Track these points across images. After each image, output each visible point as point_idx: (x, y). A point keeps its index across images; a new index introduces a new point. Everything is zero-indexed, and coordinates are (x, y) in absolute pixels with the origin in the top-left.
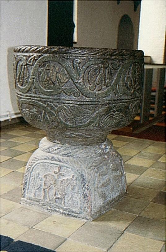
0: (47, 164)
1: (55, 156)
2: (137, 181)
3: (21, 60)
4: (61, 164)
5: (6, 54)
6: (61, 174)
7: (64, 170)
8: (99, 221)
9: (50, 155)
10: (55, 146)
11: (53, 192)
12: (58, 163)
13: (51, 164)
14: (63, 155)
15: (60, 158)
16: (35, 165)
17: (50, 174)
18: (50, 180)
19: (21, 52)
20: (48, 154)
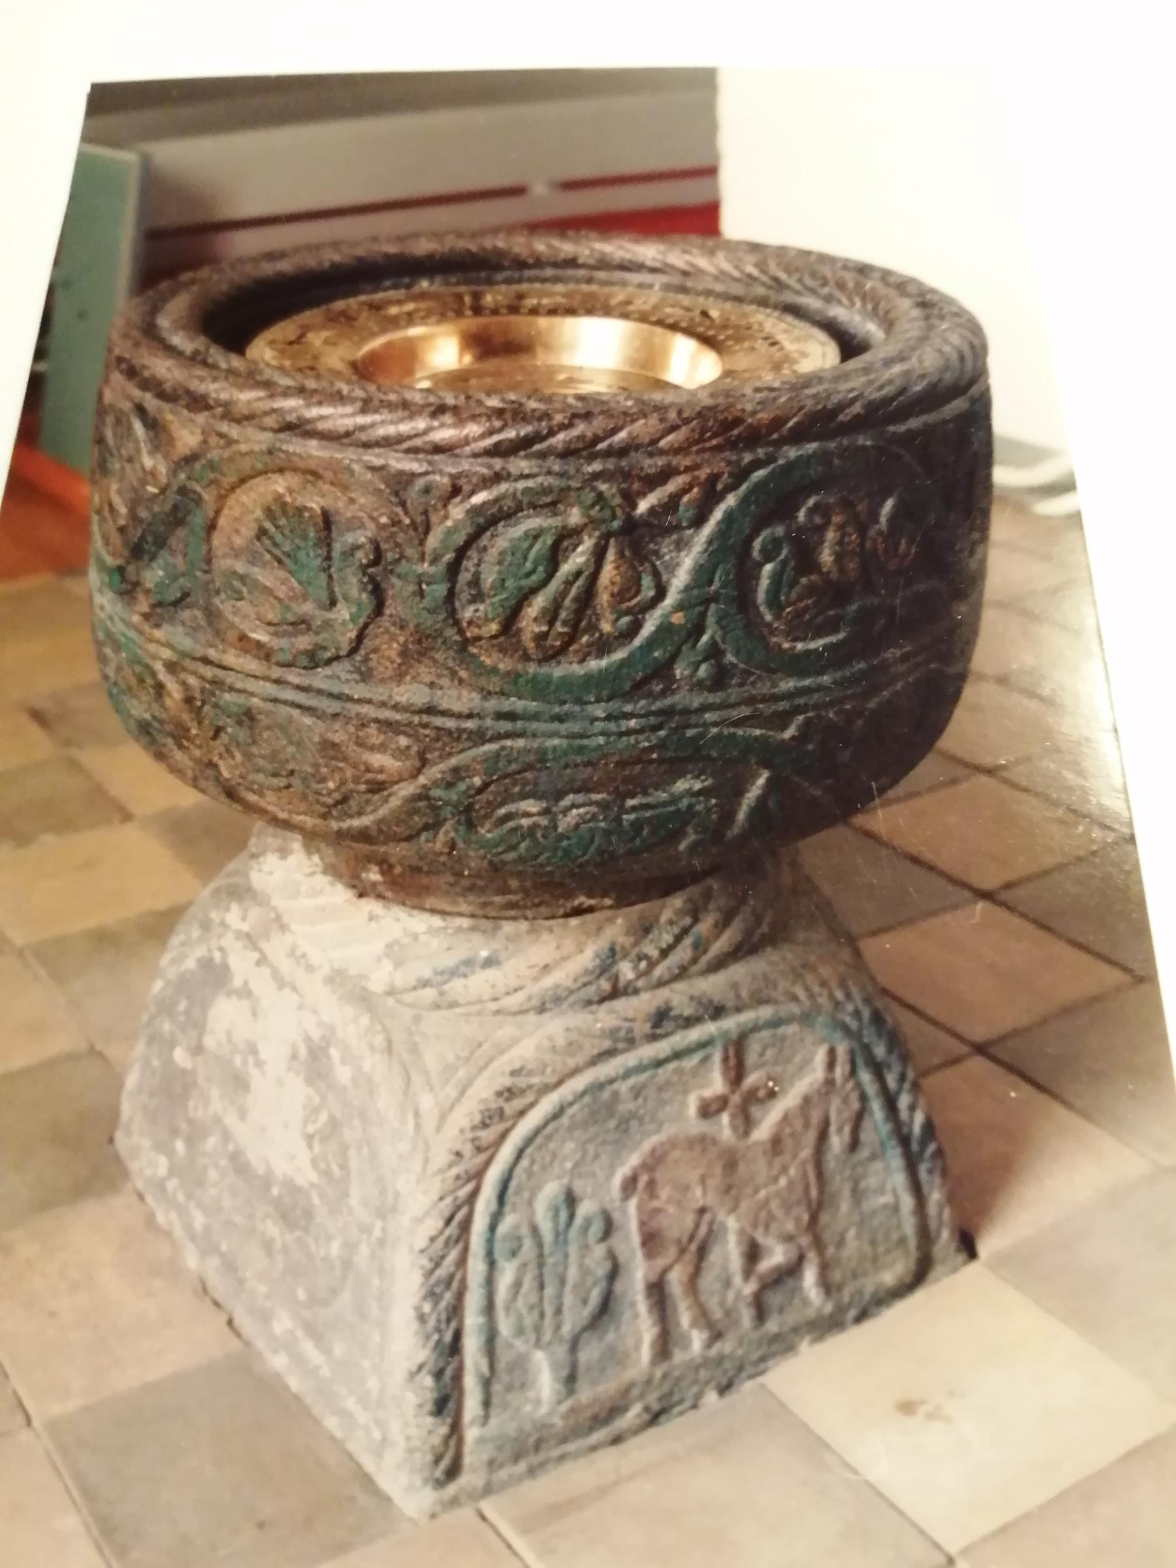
0: (624, 1087)
1: (679, 997)
2: (1010, 1043)
3: (291, 343)
4: (731, 1023)
5: (88, 89)
6: (751, 1097)
7: (762, 1054)
8: (744, 957)
9: (630, 1014)
10: (647, 930)
11: (730, 1252)
12: (710, 1028)
13: (659, 1063)
14: (719, 964)
15: (712, 985)
16: (489, 1308)
17: (673, 1143)
18: (687, 1188)
19: (530, 1087)
20: (606, 1017)
